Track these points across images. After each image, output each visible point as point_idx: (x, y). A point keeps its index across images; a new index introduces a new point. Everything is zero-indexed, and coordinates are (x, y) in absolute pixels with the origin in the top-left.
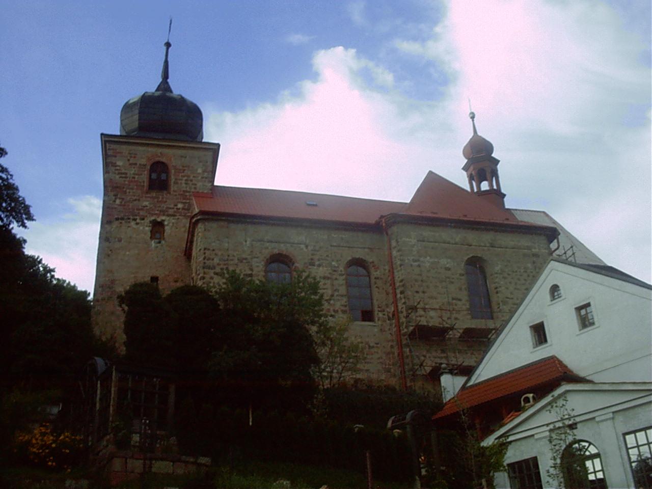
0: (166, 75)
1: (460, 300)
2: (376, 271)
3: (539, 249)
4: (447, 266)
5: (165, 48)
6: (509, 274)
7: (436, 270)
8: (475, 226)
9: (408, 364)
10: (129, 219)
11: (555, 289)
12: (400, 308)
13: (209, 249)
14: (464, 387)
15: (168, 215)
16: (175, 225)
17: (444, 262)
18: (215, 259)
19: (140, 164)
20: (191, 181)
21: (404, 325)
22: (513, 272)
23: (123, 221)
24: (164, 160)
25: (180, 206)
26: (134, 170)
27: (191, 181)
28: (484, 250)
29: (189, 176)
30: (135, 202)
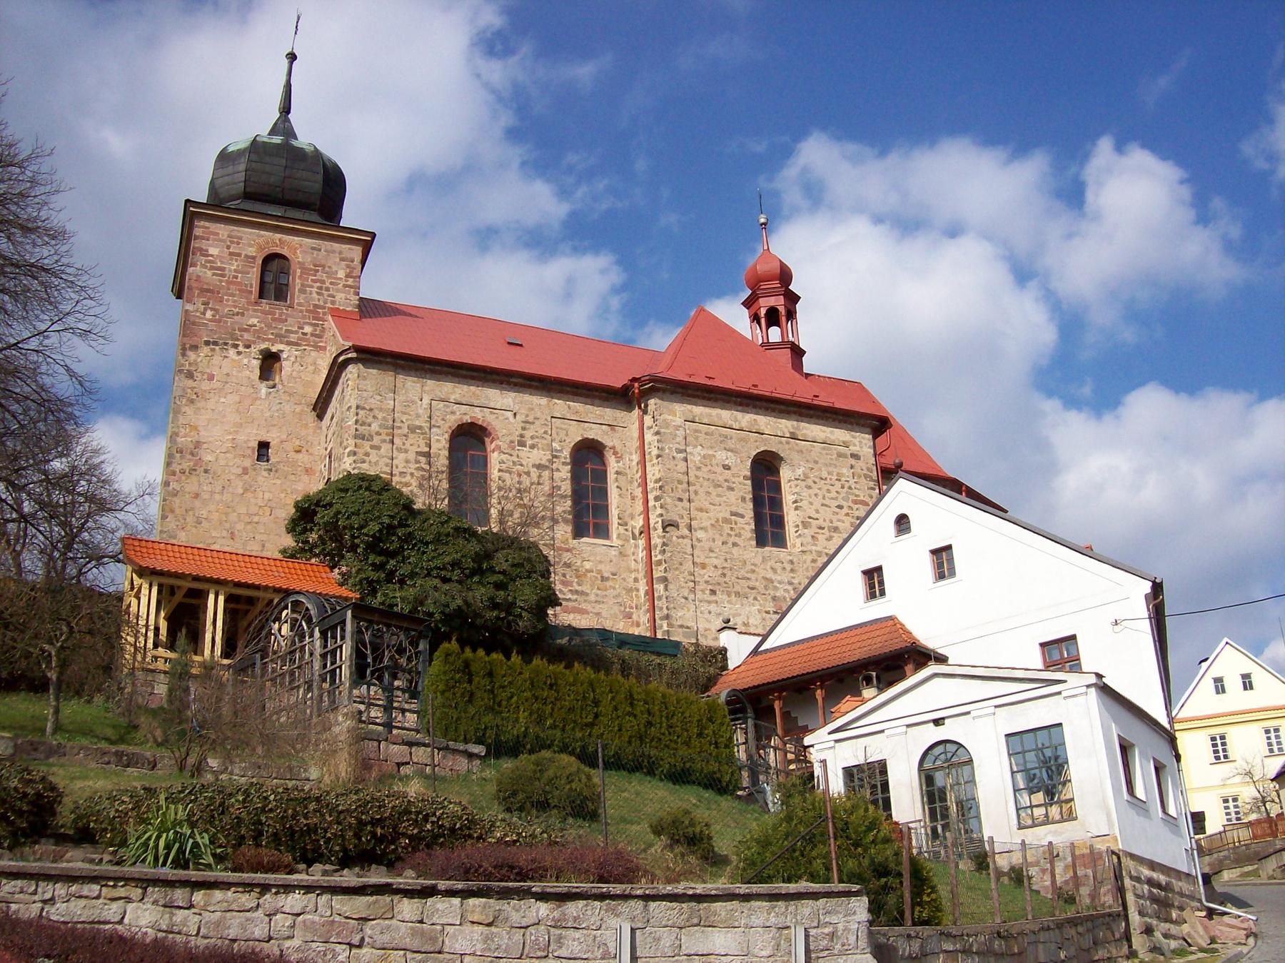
0: (286, 109)
1: (742, 516)
2: (618, 462)
3: (861, 447)
4: (726, 463)
5: (286, 62)
6: (815, 483)
7: (709, 467)
8: (772, 405)
9: (661, 609)
10: (226, 344)
11: (902, 523)
12: (652, 522)
13: (364, 408)
14: (755, 652)
15: (289, 343)
16: (298, 359)
17: (722, 456)
18: (373, 425)
19: (246, 256)
20: (328, 289)
21: (659, 548)
22: (822, 479)
23: (217, 348)
24: (285, 252)
25: (308, 329)
26: (236, 264)
27: (328, 289)
28: (781, 443)
29: (323, 282)
30: (236, 317)
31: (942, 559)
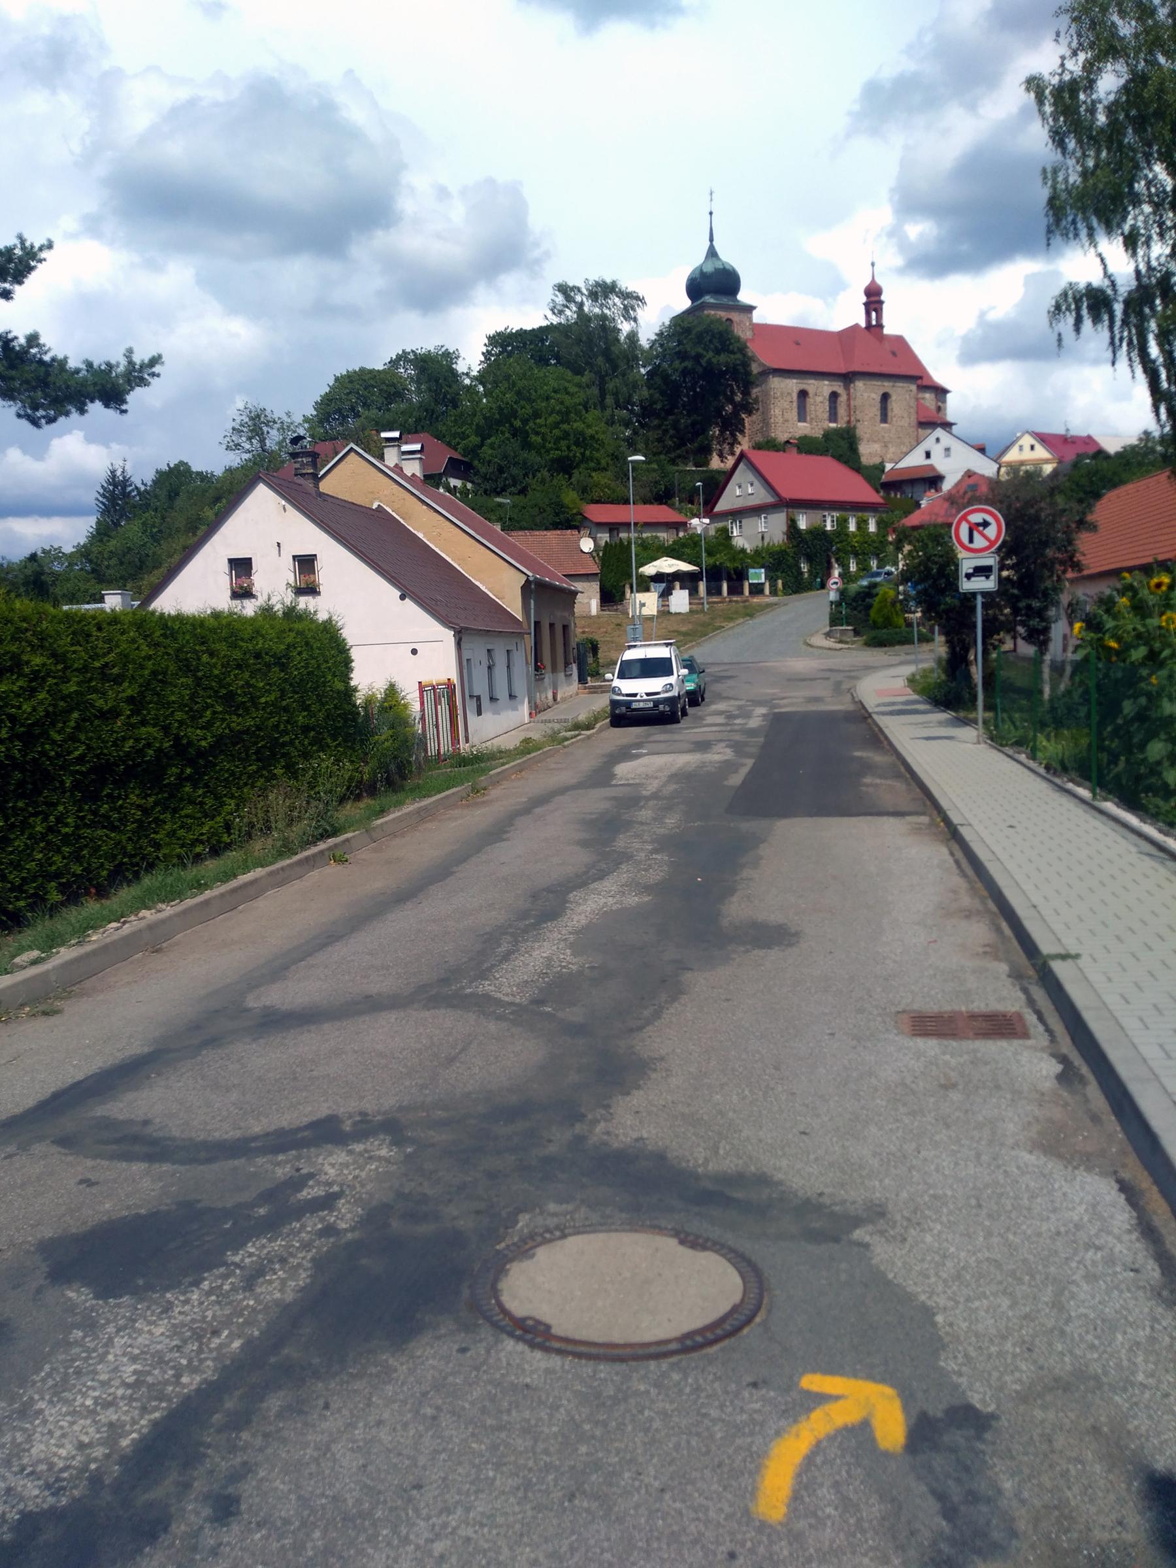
0: (711, 240)
31: (947, 450)
